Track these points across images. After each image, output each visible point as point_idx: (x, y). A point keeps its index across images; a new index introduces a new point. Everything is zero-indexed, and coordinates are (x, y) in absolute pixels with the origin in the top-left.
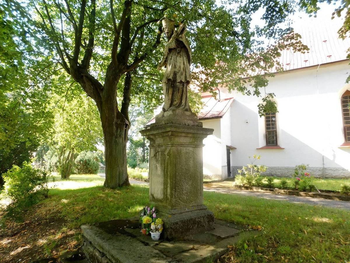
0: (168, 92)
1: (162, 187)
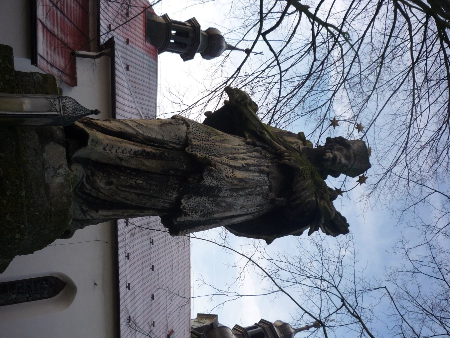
0: (148, 155)
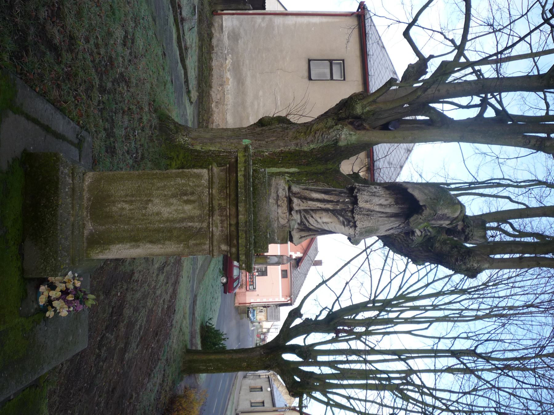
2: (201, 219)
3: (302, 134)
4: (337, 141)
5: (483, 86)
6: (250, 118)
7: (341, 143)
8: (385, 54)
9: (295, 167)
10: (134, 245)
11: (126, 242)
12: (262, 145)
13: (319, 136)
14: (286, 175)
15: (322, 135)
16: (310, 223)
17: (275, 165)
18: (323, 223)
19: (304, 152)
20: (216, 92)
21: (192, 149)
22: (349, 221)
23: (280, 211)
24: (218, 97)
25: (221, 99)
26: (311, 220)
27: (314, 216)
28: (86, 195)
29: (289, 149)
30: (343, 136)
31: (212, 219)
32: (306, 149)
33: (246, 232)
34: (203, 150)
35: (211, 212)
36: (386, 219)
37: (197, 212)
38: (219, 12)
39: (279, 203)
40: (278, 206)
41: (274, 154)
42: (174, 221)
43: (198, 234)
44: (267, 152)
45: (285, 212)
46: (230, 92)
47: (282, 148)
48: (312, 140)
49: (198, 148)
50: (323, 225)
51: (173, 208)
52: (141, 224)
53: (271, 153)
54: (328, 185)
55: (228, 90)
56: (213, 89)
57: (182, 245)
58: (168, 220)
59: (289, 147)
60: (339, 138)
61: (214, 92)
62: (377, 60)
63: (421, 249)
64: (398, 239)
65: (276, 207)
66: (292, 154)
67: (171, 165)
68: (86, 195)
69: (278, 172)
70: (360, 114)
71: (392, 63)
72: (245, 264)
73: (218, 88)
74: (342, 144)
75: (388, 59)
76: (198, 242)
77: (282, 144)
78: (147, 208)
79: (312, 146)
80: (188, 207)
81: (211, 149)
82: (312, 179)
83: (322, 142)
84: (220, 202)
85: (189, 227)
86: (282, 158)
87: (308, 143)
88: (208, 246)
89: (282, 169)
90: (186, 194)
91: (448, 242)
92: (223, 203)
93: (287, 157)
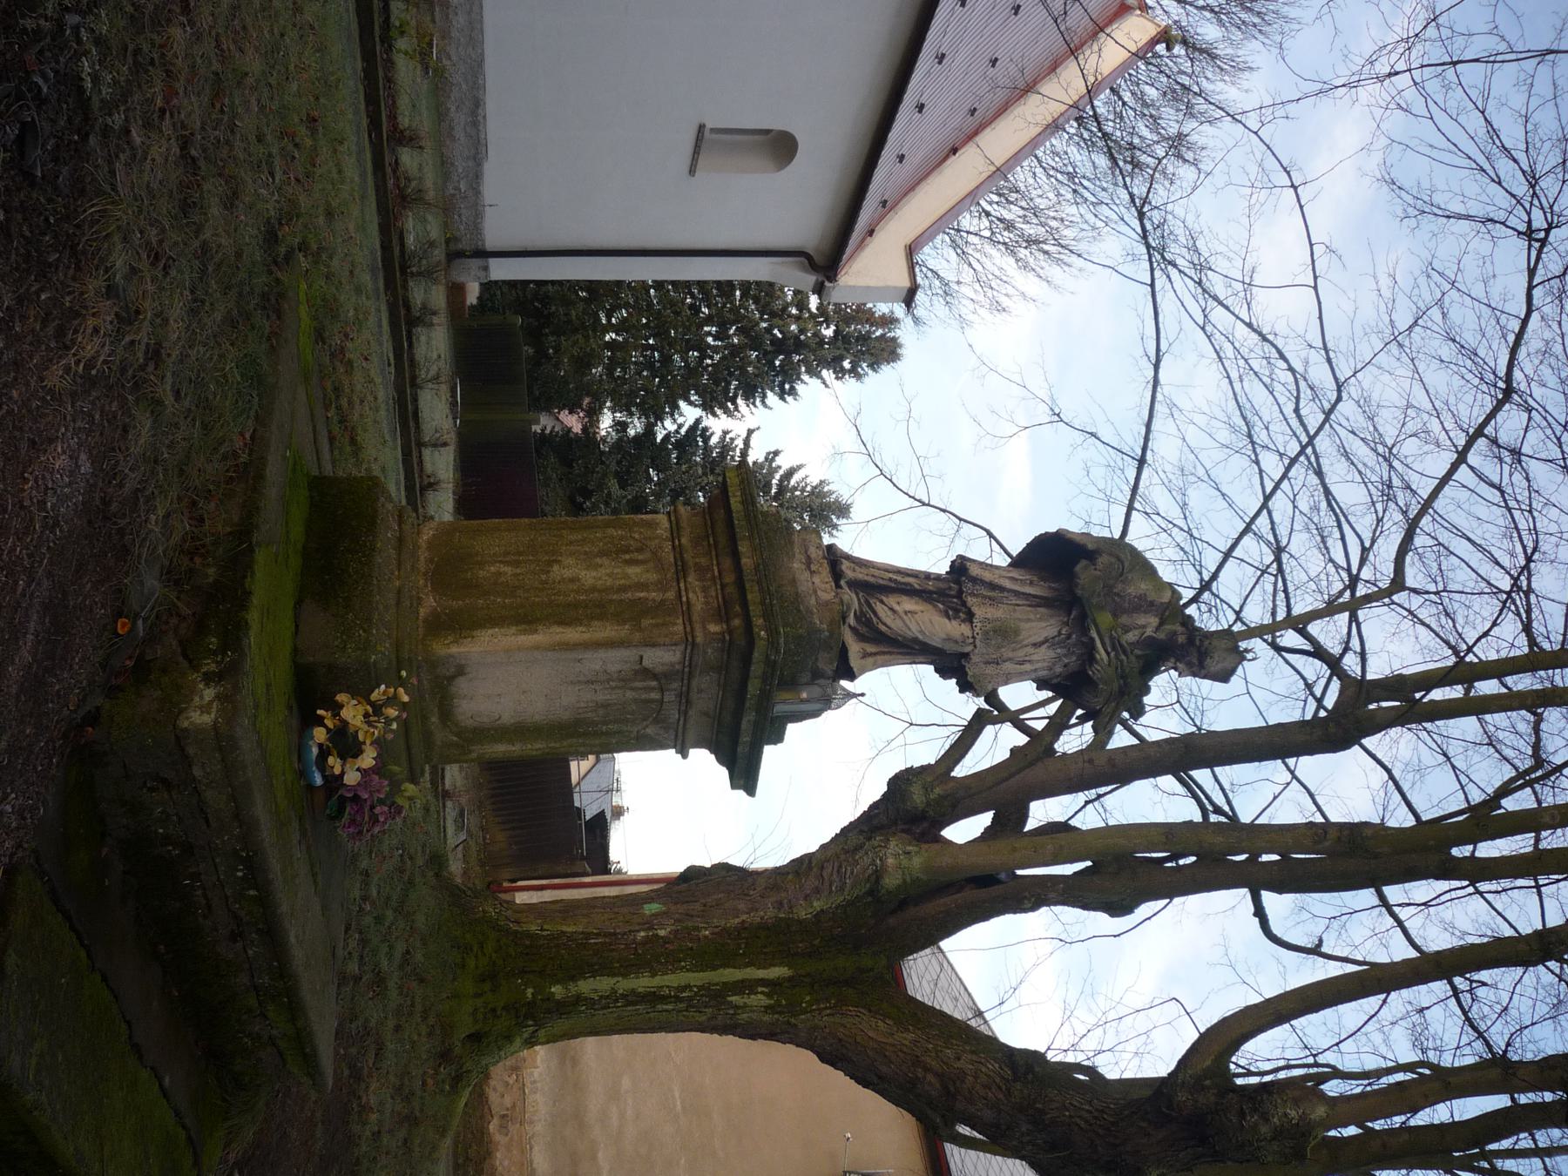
1: (507, 718)
2: (661, 586)
3: (790, 877)
4: (878, 875)
5: (1186, 747)
6: (600, 1155)
7: (887, 881)
8: (945, 964)
9: (780, 965)
10: (526, 630)
11: (508, 625)
12: (694, 913)
13: (832, 875)
14: (760, 989)
15: (838, 871)
16: (878, 618)
17: (729, 961)
18: (906, 613)
19: (800, 922)
20: (501, 1089)
21: (517, 932)
22: (957, 611)
23: (817, 580)
24: (508, 1101)
25: (514, 1106)
26: (879, 608)
27: (884, 599)
28: (423, 555)
29: (762, 918)
30: (890, 861)
31: (685, 581)
32: (803, 913)
33: (759, 582)
34: (545, 933)
35: (682, 570)
36: (1029, 609)
37: (653, 577)
38: (506, 884)
39: (813, 568)
40: (813, 573)
41: (725, 931)
42: (606, 590)
43: (659, 608)
44: (706, 929)
45: (827, 580)
46: (539, 1085)
47: (744, 917)
48: (817, 888)
49: (533, 928)
50: (905, 617)
51: (603, 571)
52: (538, 596)
53: (717, 930)
54: (870, 1011)
55: (535, 1082)
56: (492, 1083)
57: (627, 627)
58: (593, 589)
59: (762, 913)
60: (882, 865)
61: (495, 1089)
62: (927, 976)
63: (1144, 1124)
64: (1078, 1121)
65: (807, 574)
66: (768, 928)
67: (464, 966)
68: (423, 555)
69: (738, 981)
70: (921, 806)
71: (966, 989)
72: (766, 631)
73: (508, 1079)
74: (891, 881)
75: (954, 977)
76: (660, 621)
77: (742, 906)
78: (549, 572)
79: (817, 905)
80: (633, 571)
81: (565, 928)
82: (828, 1000)
83: (842, 889)
84: (697, 560)
85: (640, 599)
86: (747, 943)
87: (806, 897)
88: (681, 628)
89: (748, 970)
90: (628, 552)
91: (1208, 1082)
92: (703, 561)
93: (758, 937)
